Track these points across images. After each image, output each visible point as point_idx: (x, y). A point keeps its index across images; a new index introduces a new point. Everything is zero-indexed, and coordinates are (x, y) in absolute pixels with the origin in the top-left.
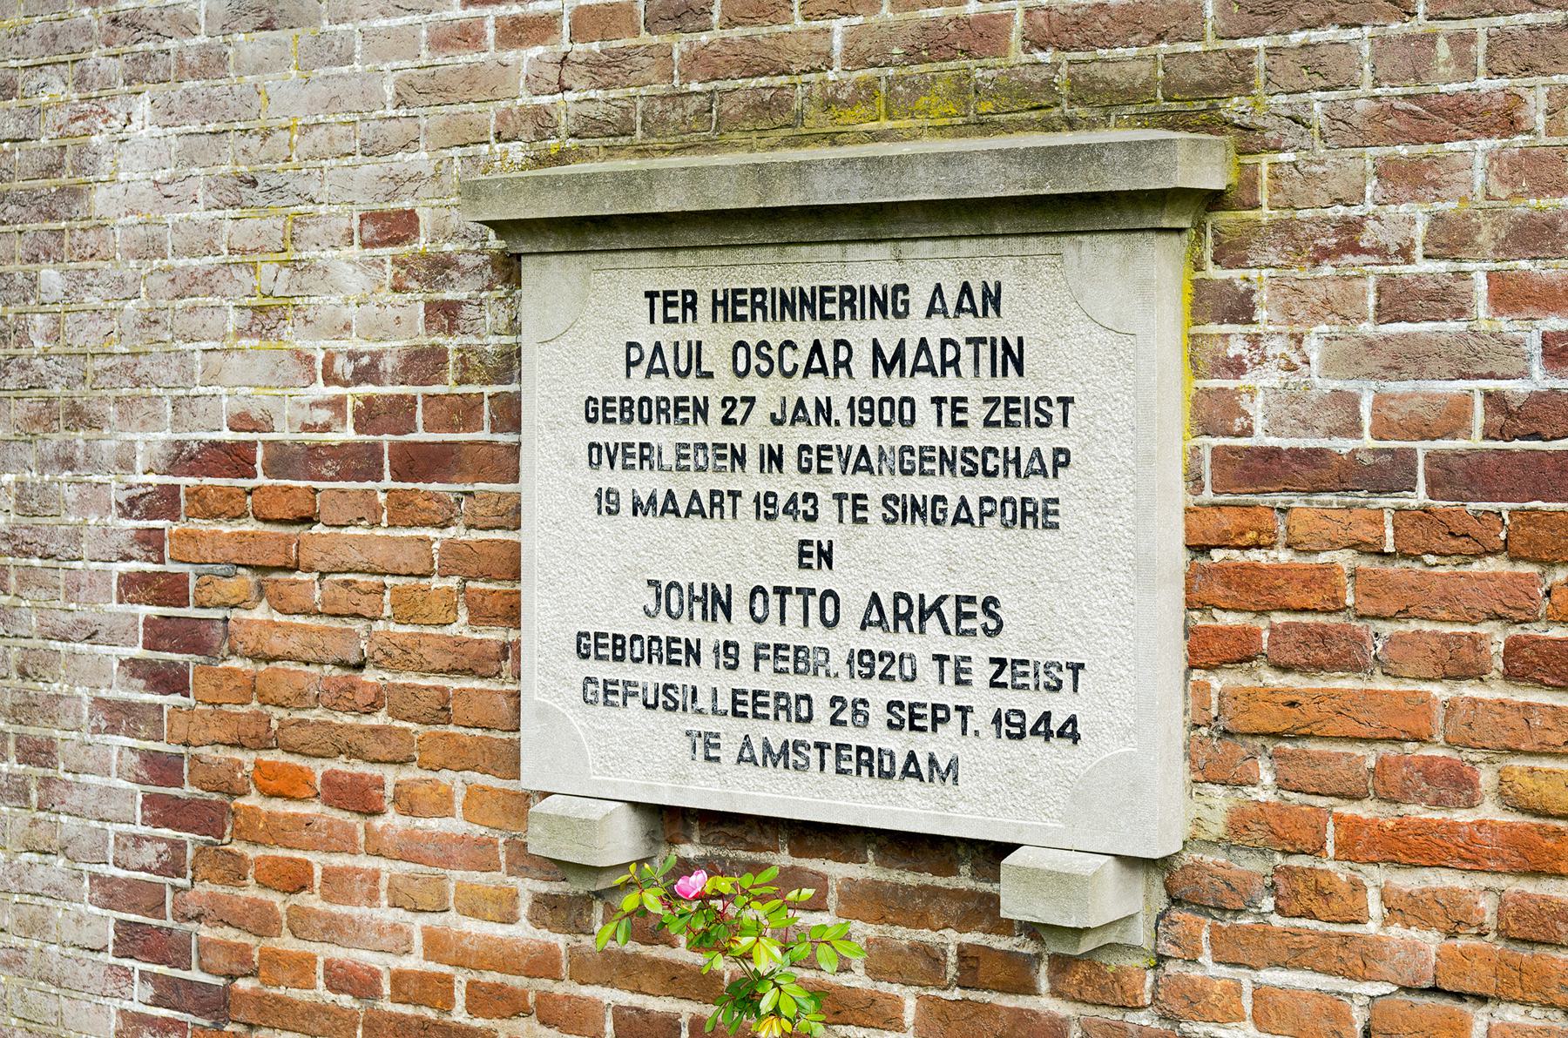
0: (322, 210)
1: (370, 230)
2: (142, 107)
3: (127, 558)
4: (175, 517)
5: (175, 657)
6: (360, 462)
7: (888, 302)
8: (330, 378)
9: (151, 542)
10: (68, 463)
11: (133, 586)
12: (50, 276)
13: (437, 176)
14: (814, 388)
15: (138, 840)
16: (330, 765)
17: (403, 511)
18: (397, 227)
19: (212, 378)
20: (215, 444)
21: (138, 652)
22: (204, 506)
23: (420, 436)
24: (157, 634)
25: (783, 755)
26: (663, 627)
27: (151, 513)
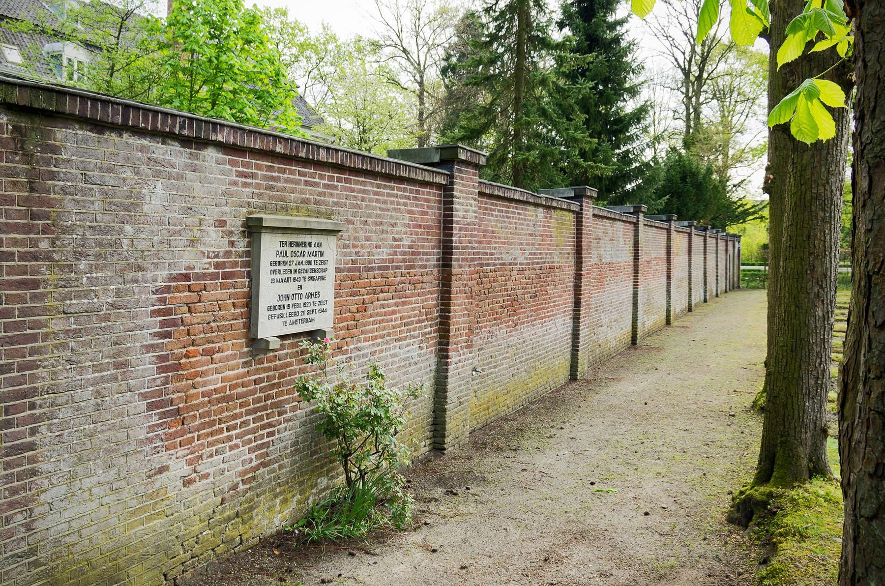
0: (207, 218)
1: (217, 223)
2: (159, 185)
3: (153, 306)
4: (169, 293)
5: (168, 329)
6: (214, 276)
7: (309, 245)
8: (208, 257)
9: (162, 301)
10: (136, 281)
11: (154, 313)
12: (128, 228)
13: (230, 213)
14: (301, 259)
15: (155, 379)
16: (204, 347)
17: (223, 286)
18: (222, 223)
19: (182, 257)
20: (181, 274)
21: (157, 330)
22: (177, 289)
23: (227, 270)
24: (163, 324)
25: (295, 323)
26: (280, 303)
27: (162, 293)
